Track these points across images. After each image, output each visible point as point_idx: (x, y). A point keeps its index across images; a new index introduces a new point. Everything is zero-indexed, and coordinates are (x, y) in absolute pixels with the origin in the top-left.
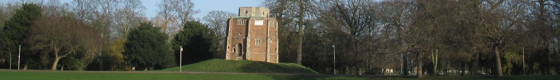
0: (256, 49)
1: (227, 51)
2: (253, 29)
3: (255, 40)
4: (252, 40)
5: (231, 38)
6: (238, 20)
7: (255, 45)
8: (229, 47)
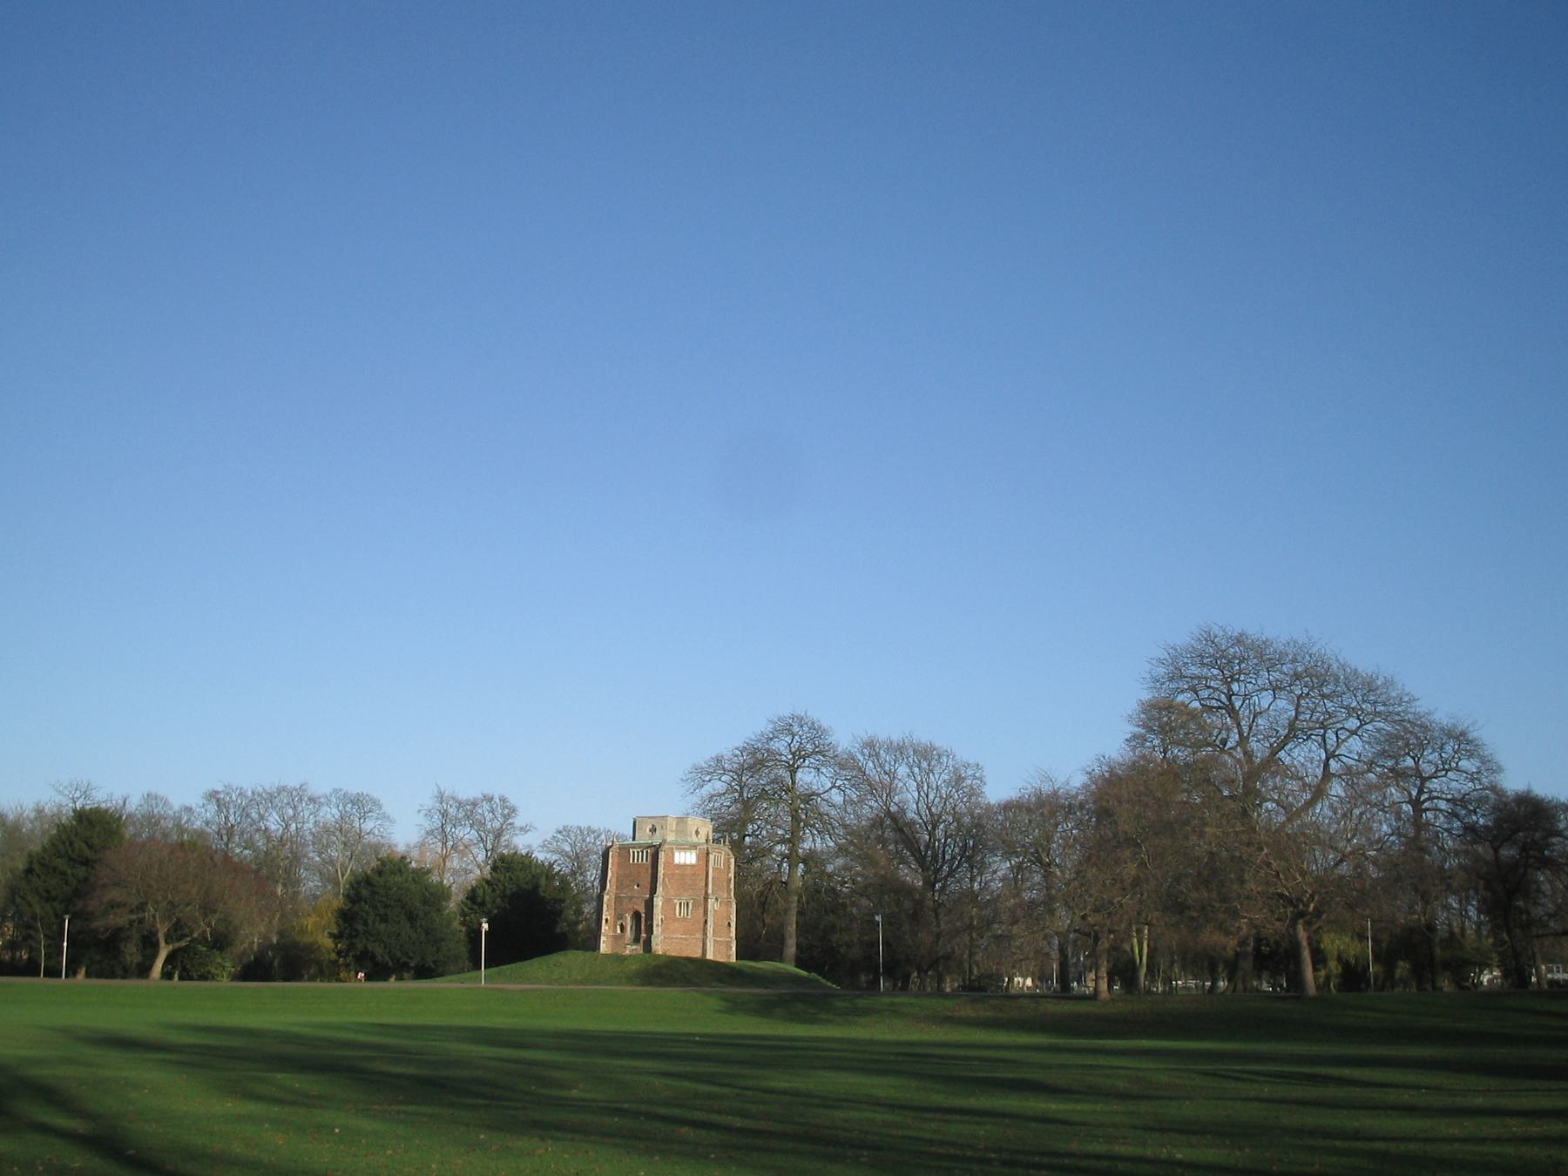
0: (677, 925)
1: (603, 931)
2: (669, 872)
3: (675, 901)
4: (668, 902)
5: (613, 897)
6: (631, 851)
7: (675, 914)
8: (607, 920)
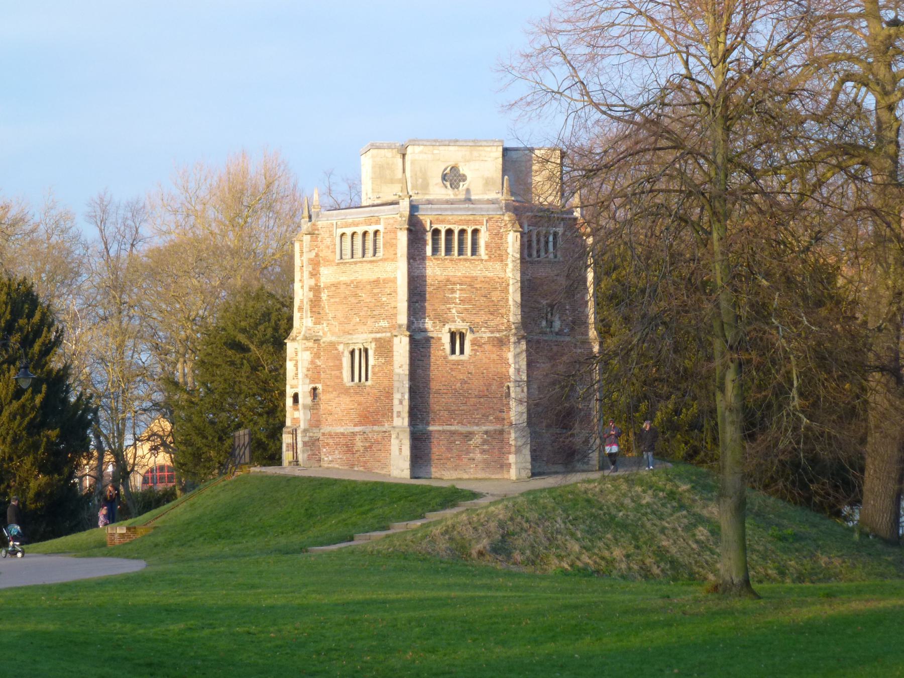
7: (340, 377)
